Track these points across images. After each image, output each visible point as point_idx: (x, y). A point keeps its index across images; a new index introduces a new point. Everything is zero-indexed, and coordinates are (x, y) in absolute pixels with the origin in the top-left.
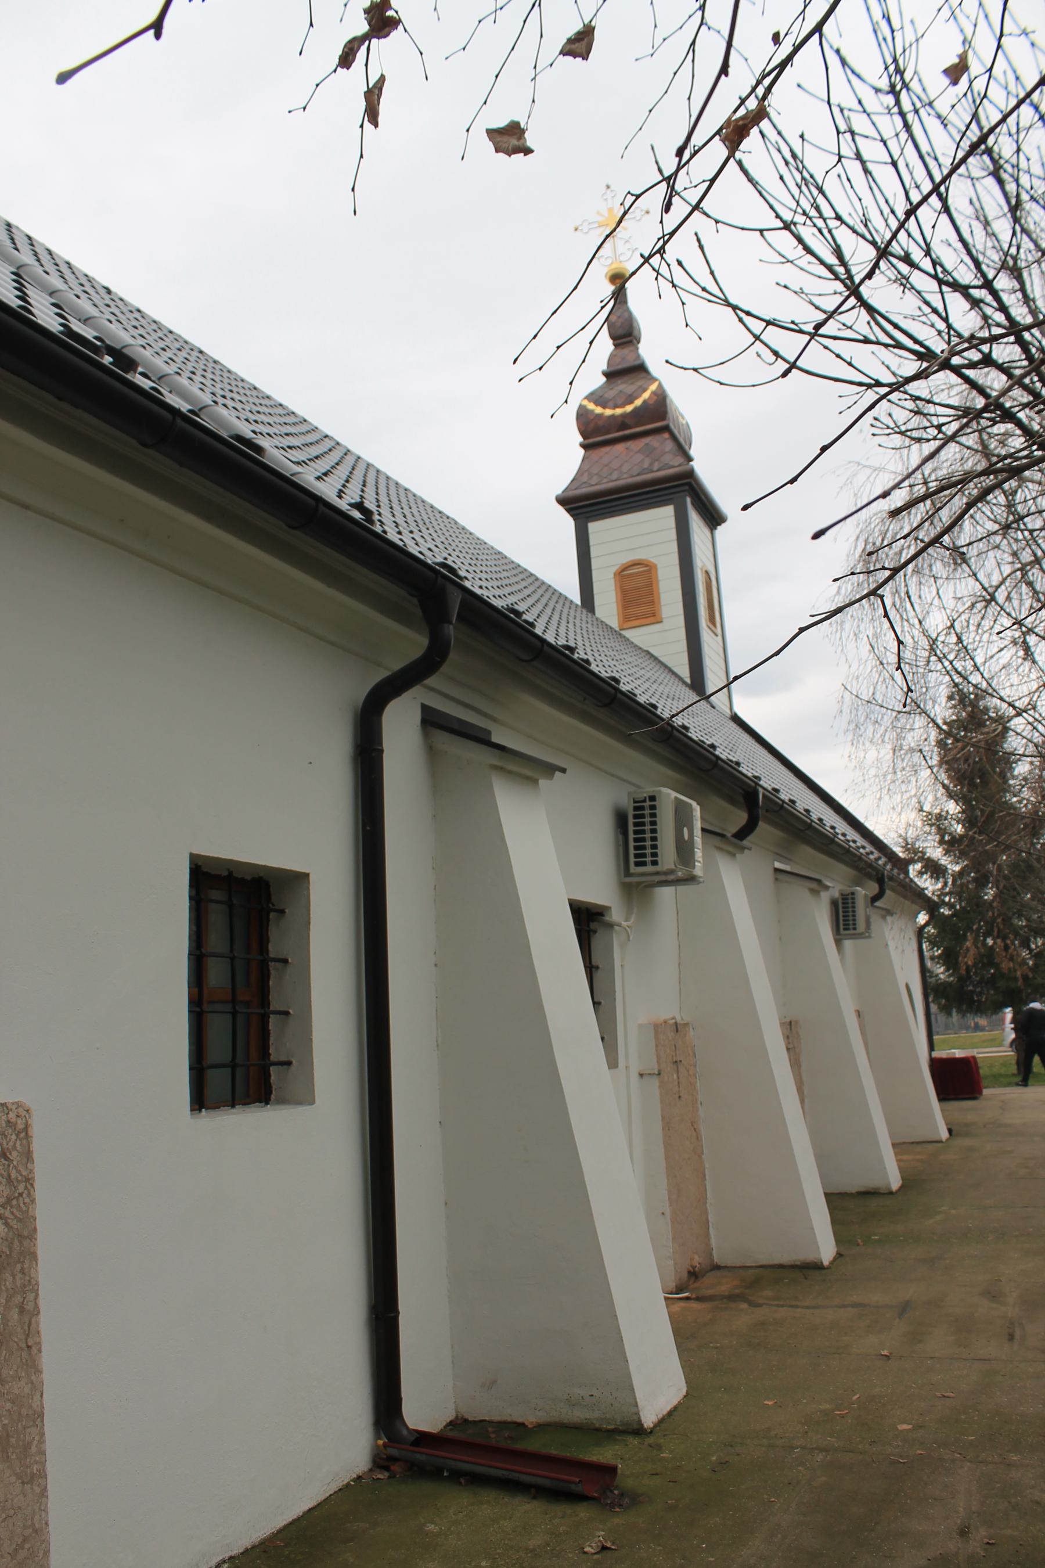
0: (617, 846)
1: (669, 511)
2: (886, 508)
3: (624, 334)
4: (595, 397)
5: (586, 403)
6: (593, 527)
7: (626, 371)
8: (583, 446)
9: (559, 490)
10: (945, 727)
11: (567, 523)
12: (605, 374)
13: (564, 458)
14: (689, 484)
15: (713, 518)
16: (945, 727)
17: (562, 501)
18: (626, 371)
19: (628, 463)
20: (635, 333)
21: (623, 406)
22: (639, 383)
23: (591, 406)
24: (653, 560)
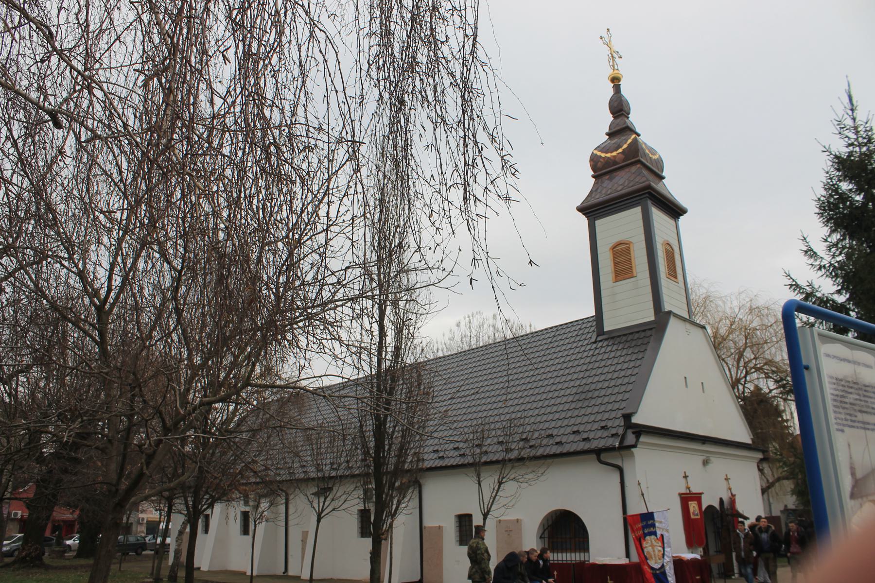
0: (439, 565)
2: (611, 283)
3: (619, 108)
4: (602, 148)
5: (595, 152)
6: (598, 223)
8: (593, 176)
9: (579, 200)
10: (740, 519)
11: (583, 221)
12: (607, 134)
13: (583, 184)
14: (649, 193)
15: (675, 211)
16: (740, 519)
17: (581, 209)
19: (622, 183)
20: (625, 109)
21: (607, 153)
22: (623, 138)
23: (599, 153)
24: (630, 240)
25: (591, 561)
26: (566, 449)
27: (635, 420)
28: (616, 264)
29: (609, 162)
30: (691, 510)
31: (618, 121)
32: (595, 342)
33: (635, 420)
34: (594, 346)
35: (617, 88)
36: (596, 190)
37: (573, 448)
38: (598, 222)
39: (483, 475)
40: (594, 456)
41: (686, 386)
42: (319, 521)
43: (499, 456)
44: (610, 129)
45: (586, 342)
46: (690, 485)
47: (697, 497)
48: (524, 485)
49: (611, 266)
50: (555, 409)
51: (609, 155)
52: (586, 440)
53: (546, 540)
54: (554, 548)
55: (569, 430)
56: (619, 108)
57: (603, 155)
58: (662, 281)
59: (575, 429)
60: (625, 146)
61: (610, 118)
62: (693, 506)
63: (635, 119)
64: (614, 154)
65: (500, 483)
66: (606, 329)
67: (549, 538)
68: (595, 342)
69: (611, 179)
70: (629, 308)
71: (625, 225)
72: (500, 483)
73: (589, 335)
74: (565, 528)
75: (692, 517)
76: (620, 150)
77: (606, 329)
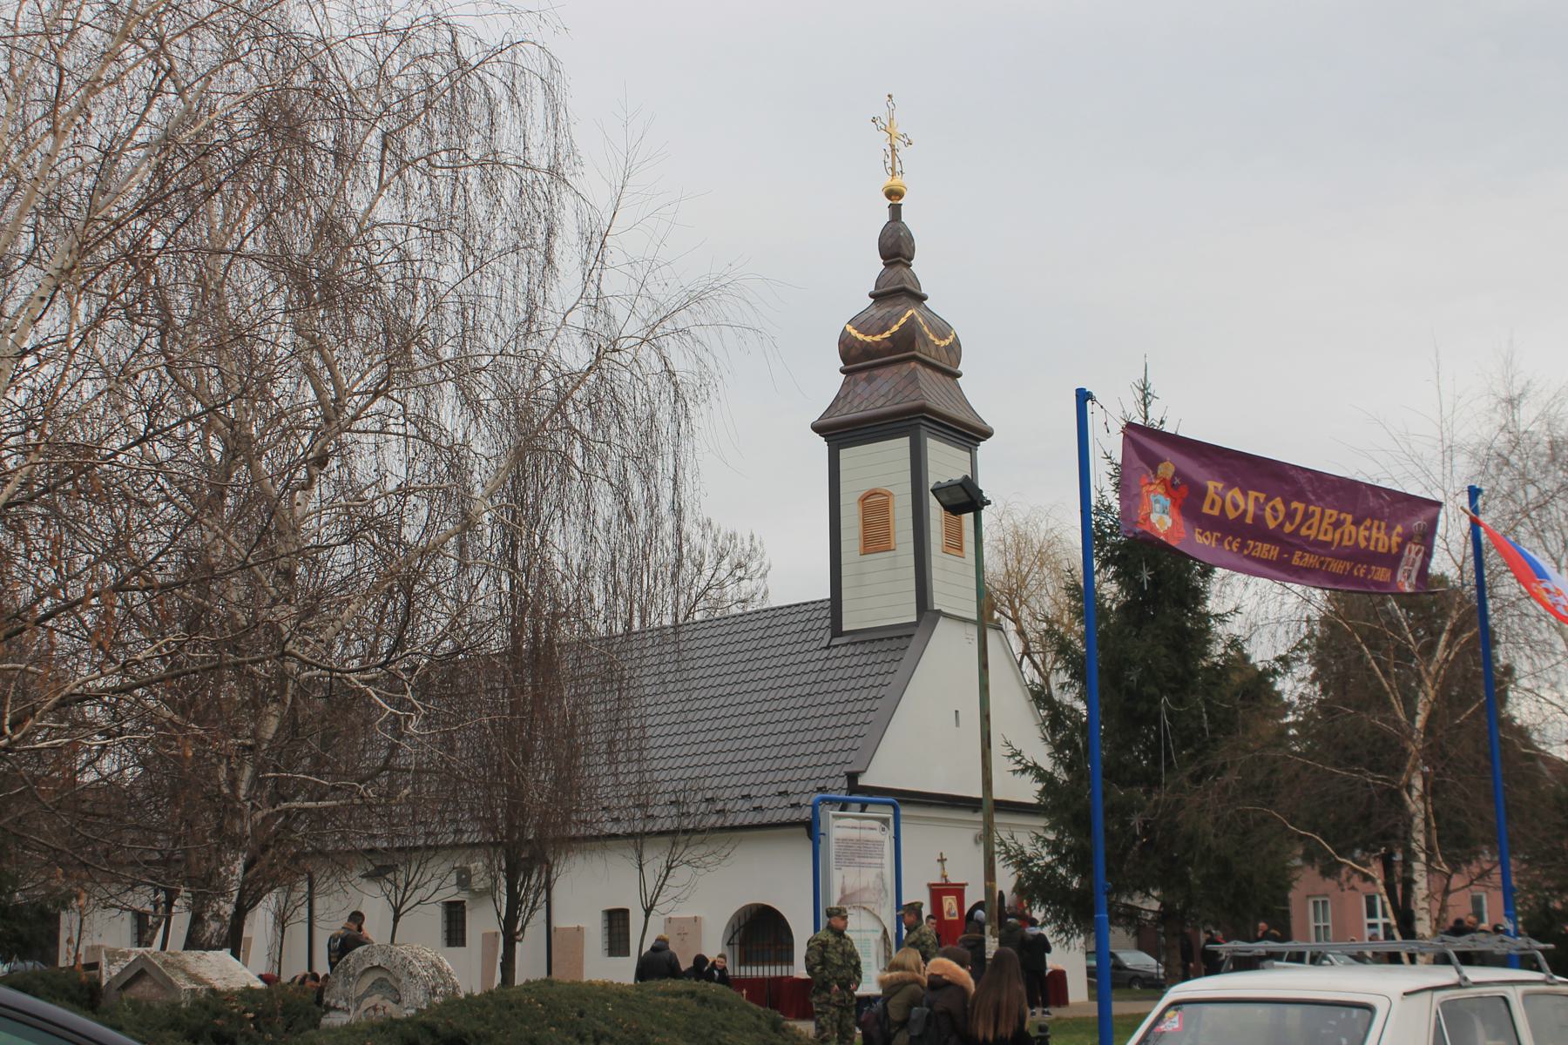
1: (905, 442)
3: (896, 248)
4: (858, 322)
5: (849, 328)
7: (897, 287)
8: (842, 371)
11: (821, 445)
12: (871, 296)
13: (824, 381)
15: (970, 434)
17: (817, 428)
18: (897, 287)
19: (882, 394)
23: (854, 332)
25: (585, 979)
26: (767, 817)
27: (863, 781)
28: (866, 525)
29: (868, 351)
30: (946, 908)
31: (892, 272)
32: (828, 647)
33: (863, 781)
34: (826, 653)
35: (896, 211)
36: (846, 397)
37: (777, 817)
38: (844, 453)
39: (647, 856)
40: (803, 830)
41: (957, 724)
42: (396, 919)
43: (668, 825)
44: (877, 287)
45: (815, 645)
46: (947, 872)
47: (958, 891)
48: (700, 871)
49: (854, 526)
50: (809, 736)
51: (868, 339)
52: (758, 809)
53: (737, 947)
54: (745, 960)
55: (774, 789)
56: (896, 248)
57: (860, 337)
58: (933, 559)
59: (782, 788)
60: (895, 328)
61: (878, 265)
62: (949, 902)
63: (921, 267)
64: (878, 338)
65: (669, 868)
66: (845, 628)
67: (741, 944)
68: (828, 647)
69: (869, 380)
70: (880, 598)
71: (881, 465)
72: (669, 868)
73: (821, 633)
74: (760, 929)
75: (946, 917)
76: (887, 334)
77: (845, 628)
